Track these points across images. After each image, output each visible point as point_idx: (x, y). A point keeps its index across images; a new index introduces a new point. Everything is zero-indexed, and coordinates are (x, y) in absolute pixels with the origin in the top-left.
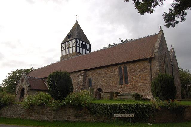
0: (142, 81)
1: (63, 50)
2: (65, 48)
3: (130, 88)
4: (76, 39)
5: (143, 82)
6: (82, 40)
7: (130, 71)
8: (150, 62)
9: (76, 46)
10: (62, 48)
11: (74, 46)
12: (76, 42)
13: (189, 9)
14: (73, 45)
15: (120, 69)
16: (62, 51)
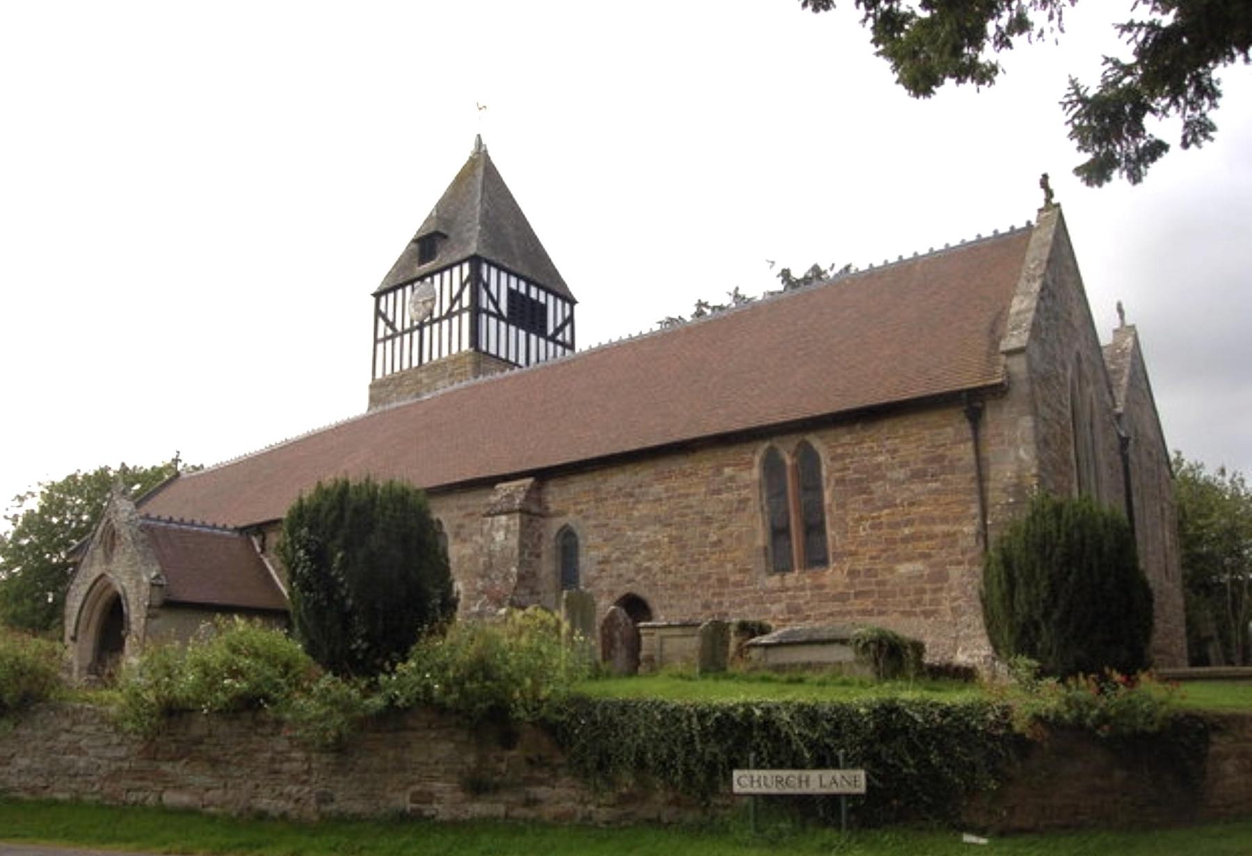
0: (923, 546)
2: (398, 326)
3: (841, 598)
5: (925, 556)
7: (841, 481)
8: (975, 418)
11: (462, 310)
12: (476, 281)
14: (453, 302)
15: (772, 466)
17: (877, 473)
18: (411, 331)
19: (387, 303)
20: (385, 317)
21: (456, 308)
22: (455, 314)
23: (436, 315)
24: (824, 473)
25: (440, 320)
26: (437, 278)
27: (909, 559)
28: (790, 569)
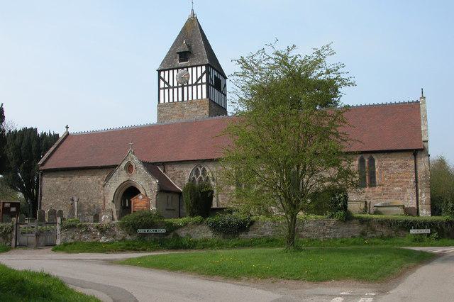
0: (401, 184)
1: (164, 88)
2: (171, 84)
4: (207, 66)
5: (401, 186)
6: (176, 66)
7: (381, 167)
8: (415, 155)
9: (208, 84)
10: (162, 82)
11: (202, 84)
13: (329, 62)
14: (198, 80)
15: (362, 161)
16: (162, 91)
17: (390, 165)
18: (178, 87)
19: (165, 75)
20: (164, 80)
21: (200, 82)
22: (199, 84)
23: (190, 83)
24: (376, 164)
25: (192, 85)
26: (190, 69)
27: (397, 186)
28: (366, 187)
